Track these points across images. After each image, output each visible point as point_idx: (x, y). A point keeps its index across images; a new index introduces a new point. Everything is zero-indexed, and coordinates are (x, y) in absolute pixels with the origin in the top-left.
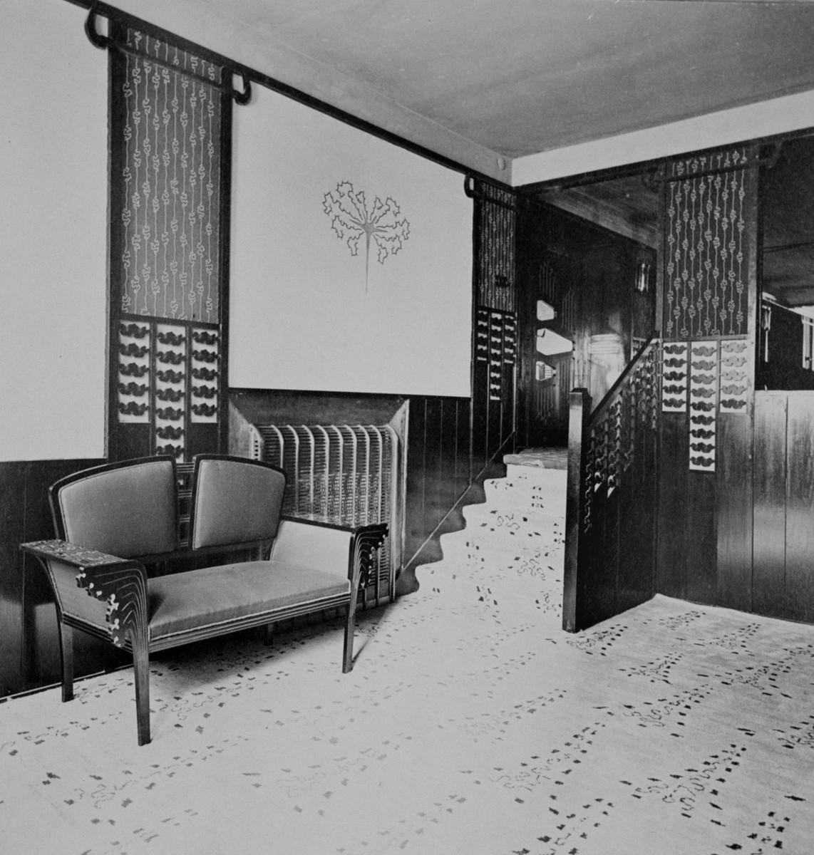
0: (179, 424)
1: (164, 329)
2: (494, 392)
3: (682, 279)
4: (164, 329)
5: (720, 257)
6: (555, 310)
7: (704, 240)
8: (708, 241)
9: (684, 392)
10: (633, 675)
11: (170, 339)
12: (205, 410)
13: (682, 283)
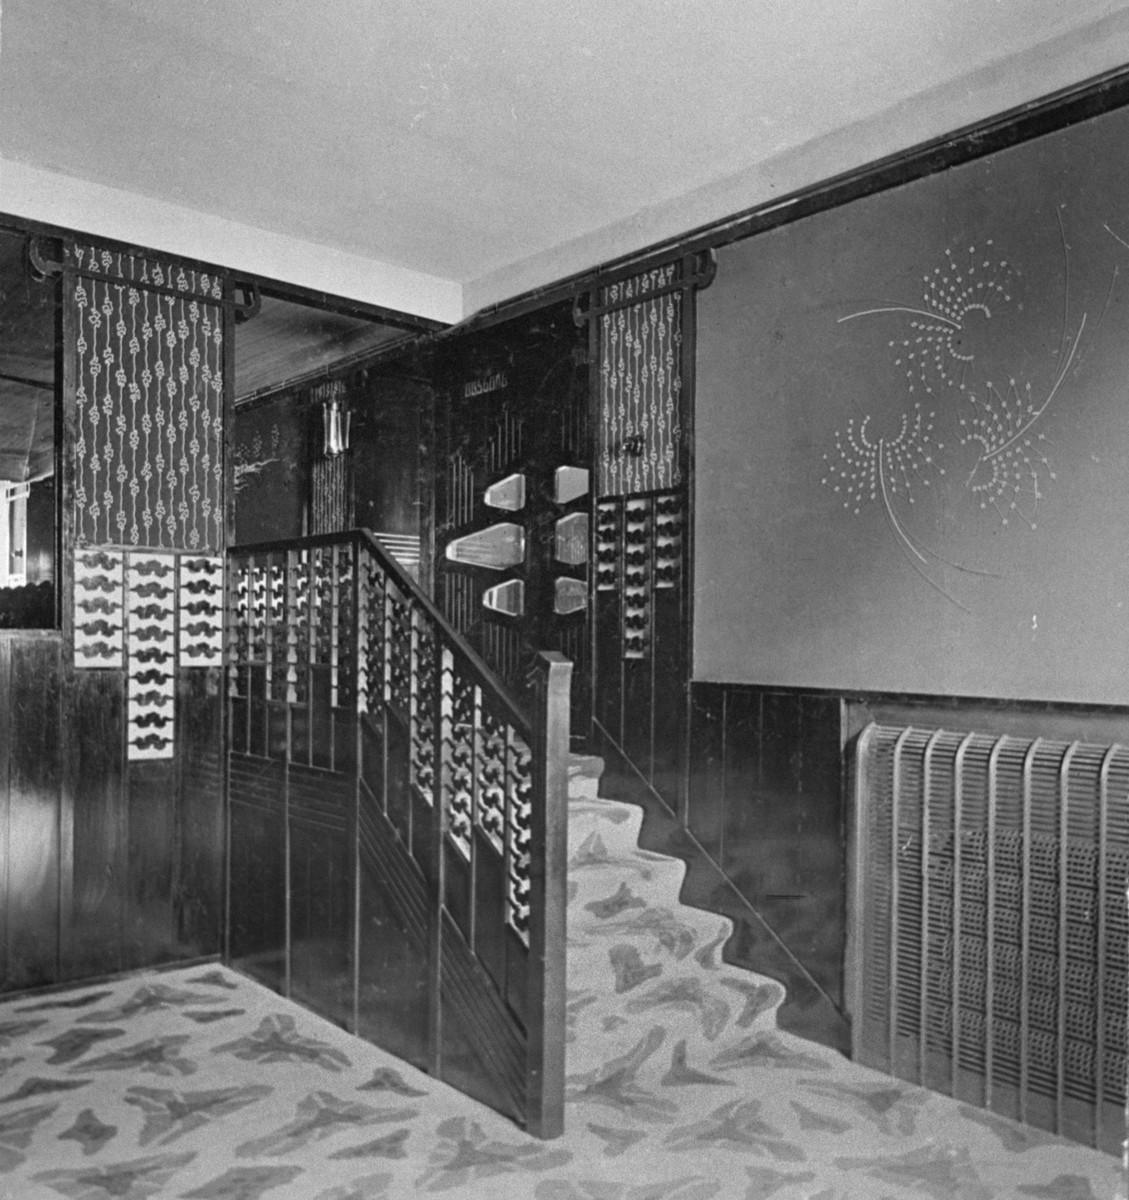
2: (635, 644)
3: (177, 335)
5: (115, 352)
6: (576, 566)
7: (141, 387)
8: (135, 384)
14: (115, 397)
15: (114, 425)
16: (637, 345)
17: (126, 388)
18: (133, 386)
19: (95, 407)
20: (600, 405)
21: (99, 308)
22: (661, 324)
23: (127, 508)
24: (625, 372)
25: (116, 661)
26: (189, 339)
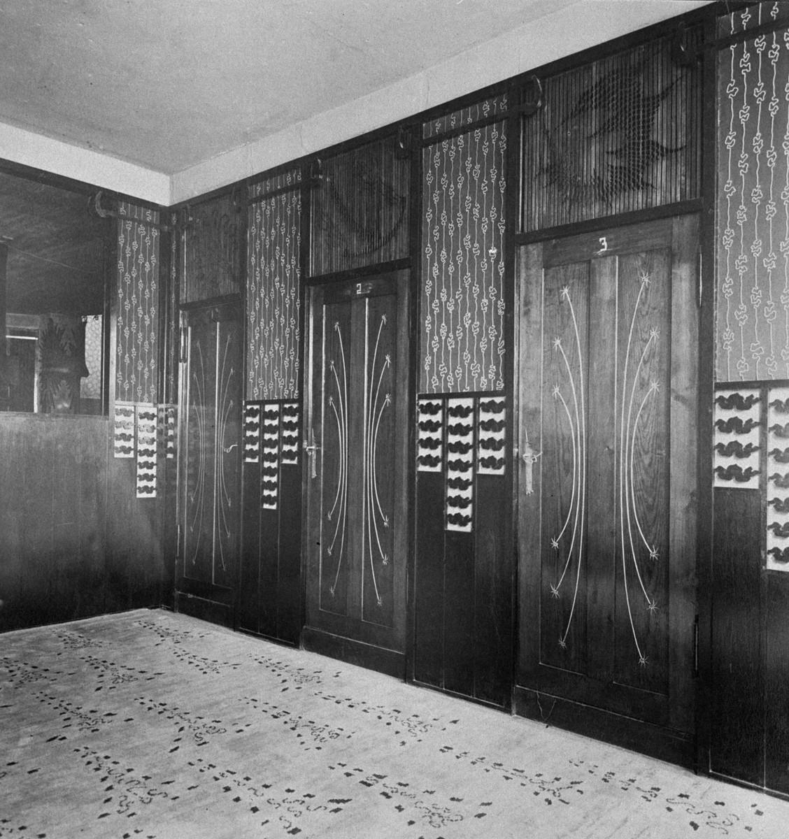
0: (467, 475)
1: (453, 403)
4: (453, 403)
9: (132, 452)
10: (648, 788)
11: (460, 412)
12: (490, 462)
13: (751, 263)
14: (137, 322)
15: (137, 338)
16: (468, 244)
17: (143, 318)
18: (146, 317)
19: (127, 328)
20: (117, 289)
21: (130, 273)
22: (444, 262)
23: (143, 385)
24: (285, 267)
25: (753, 483)
26: (138, 276)
